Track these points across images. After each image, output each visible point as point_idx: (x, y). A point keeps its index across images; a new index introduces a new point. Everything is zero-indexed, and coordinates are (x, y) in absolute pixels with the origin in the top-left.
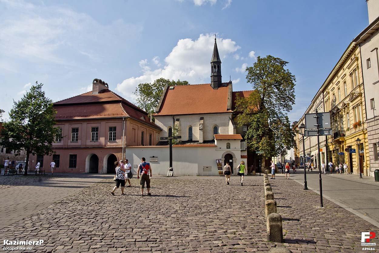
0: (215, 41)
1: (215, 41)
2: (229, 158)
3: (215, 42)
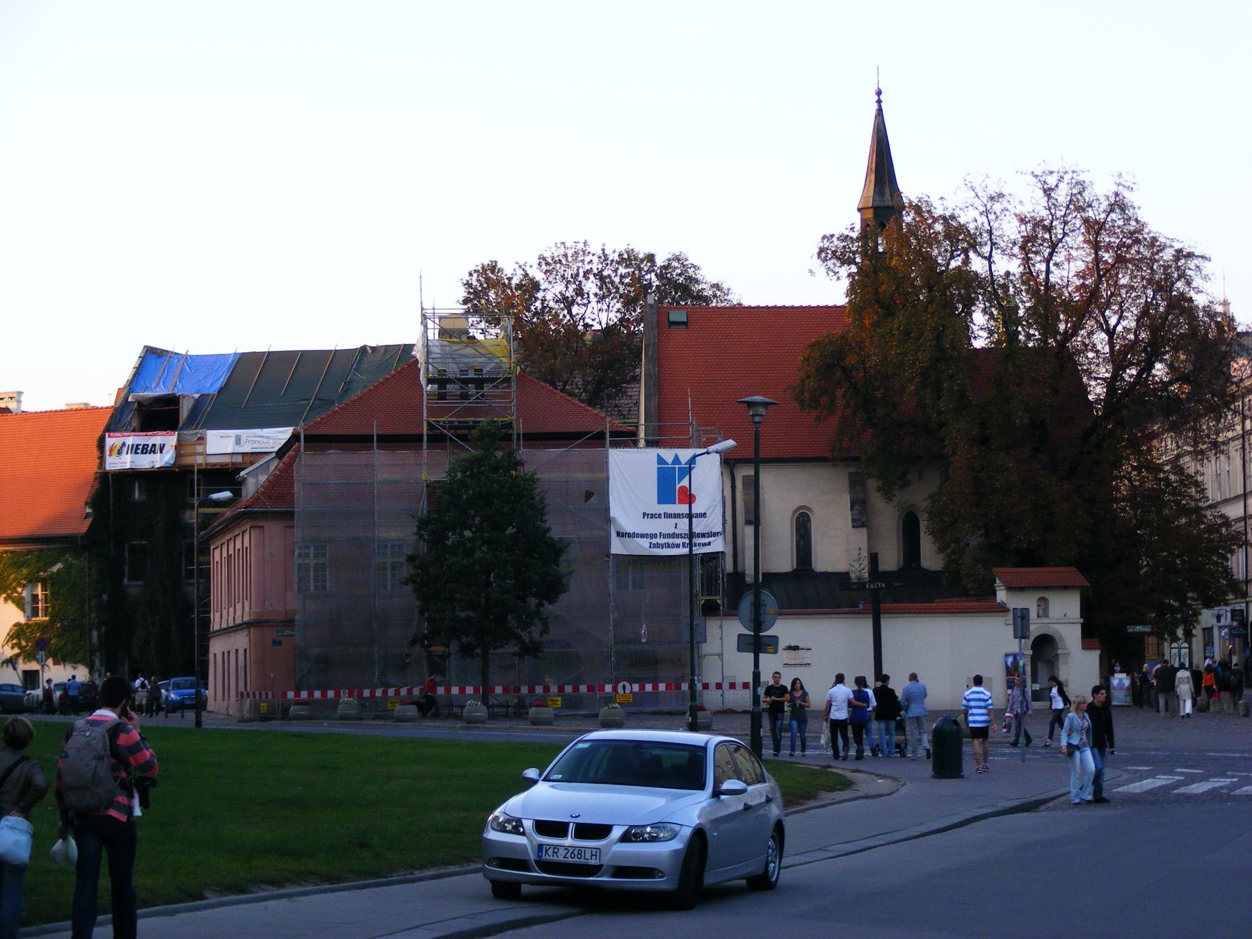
0: (879, 102)
1: (879, 102)
2: (1045, 647)
3: (875, 106)
